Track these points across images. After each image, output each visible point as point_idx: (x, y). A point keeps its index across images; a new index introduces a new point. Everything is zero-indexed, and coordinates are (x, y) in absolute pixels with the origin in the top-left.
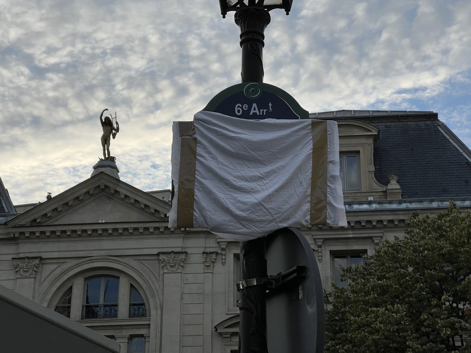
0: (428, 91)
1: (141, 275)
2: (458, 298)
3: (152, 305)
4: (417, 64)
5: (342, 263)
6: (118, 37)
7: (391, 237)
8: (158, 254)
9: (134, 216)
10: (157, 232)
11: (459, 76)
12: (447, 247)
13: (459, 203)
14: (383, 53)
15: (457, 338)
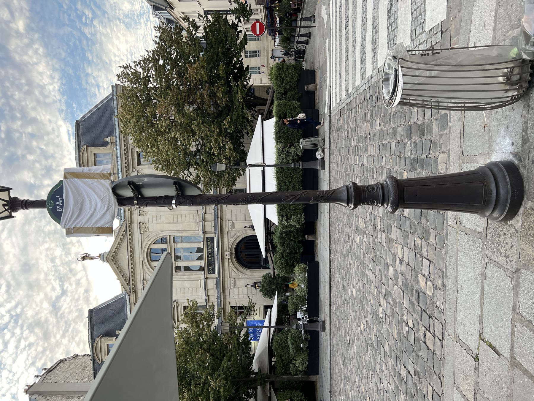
0: (69, 129)
1: (150, 240)
2: (155, 117)
3: (162, 235)
4: (56, 133)
5: (142, 160)
6: (46, 261)
7: (131, 142)
8: (141, 234)
9: (125, 244)
10: (131, 235)
11: (62, 116)
12: (134, 120)
13: (116, 114)
14: (51, 148)
15: (171, 118)
